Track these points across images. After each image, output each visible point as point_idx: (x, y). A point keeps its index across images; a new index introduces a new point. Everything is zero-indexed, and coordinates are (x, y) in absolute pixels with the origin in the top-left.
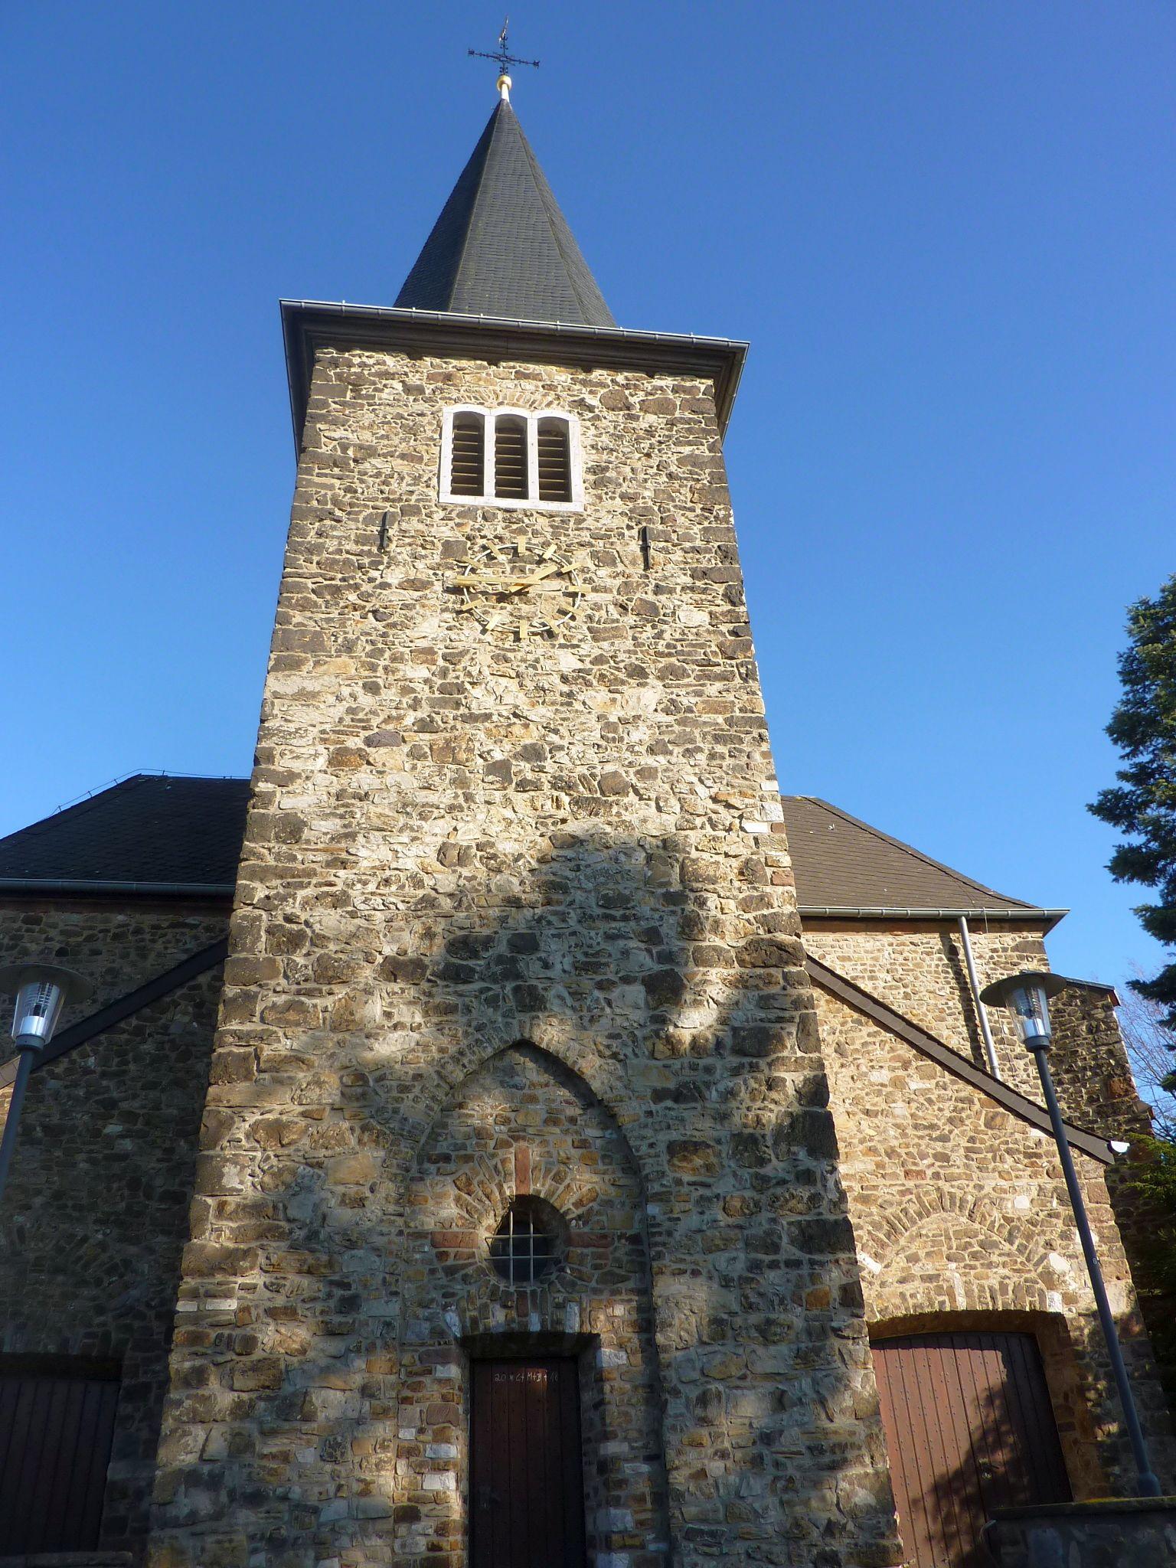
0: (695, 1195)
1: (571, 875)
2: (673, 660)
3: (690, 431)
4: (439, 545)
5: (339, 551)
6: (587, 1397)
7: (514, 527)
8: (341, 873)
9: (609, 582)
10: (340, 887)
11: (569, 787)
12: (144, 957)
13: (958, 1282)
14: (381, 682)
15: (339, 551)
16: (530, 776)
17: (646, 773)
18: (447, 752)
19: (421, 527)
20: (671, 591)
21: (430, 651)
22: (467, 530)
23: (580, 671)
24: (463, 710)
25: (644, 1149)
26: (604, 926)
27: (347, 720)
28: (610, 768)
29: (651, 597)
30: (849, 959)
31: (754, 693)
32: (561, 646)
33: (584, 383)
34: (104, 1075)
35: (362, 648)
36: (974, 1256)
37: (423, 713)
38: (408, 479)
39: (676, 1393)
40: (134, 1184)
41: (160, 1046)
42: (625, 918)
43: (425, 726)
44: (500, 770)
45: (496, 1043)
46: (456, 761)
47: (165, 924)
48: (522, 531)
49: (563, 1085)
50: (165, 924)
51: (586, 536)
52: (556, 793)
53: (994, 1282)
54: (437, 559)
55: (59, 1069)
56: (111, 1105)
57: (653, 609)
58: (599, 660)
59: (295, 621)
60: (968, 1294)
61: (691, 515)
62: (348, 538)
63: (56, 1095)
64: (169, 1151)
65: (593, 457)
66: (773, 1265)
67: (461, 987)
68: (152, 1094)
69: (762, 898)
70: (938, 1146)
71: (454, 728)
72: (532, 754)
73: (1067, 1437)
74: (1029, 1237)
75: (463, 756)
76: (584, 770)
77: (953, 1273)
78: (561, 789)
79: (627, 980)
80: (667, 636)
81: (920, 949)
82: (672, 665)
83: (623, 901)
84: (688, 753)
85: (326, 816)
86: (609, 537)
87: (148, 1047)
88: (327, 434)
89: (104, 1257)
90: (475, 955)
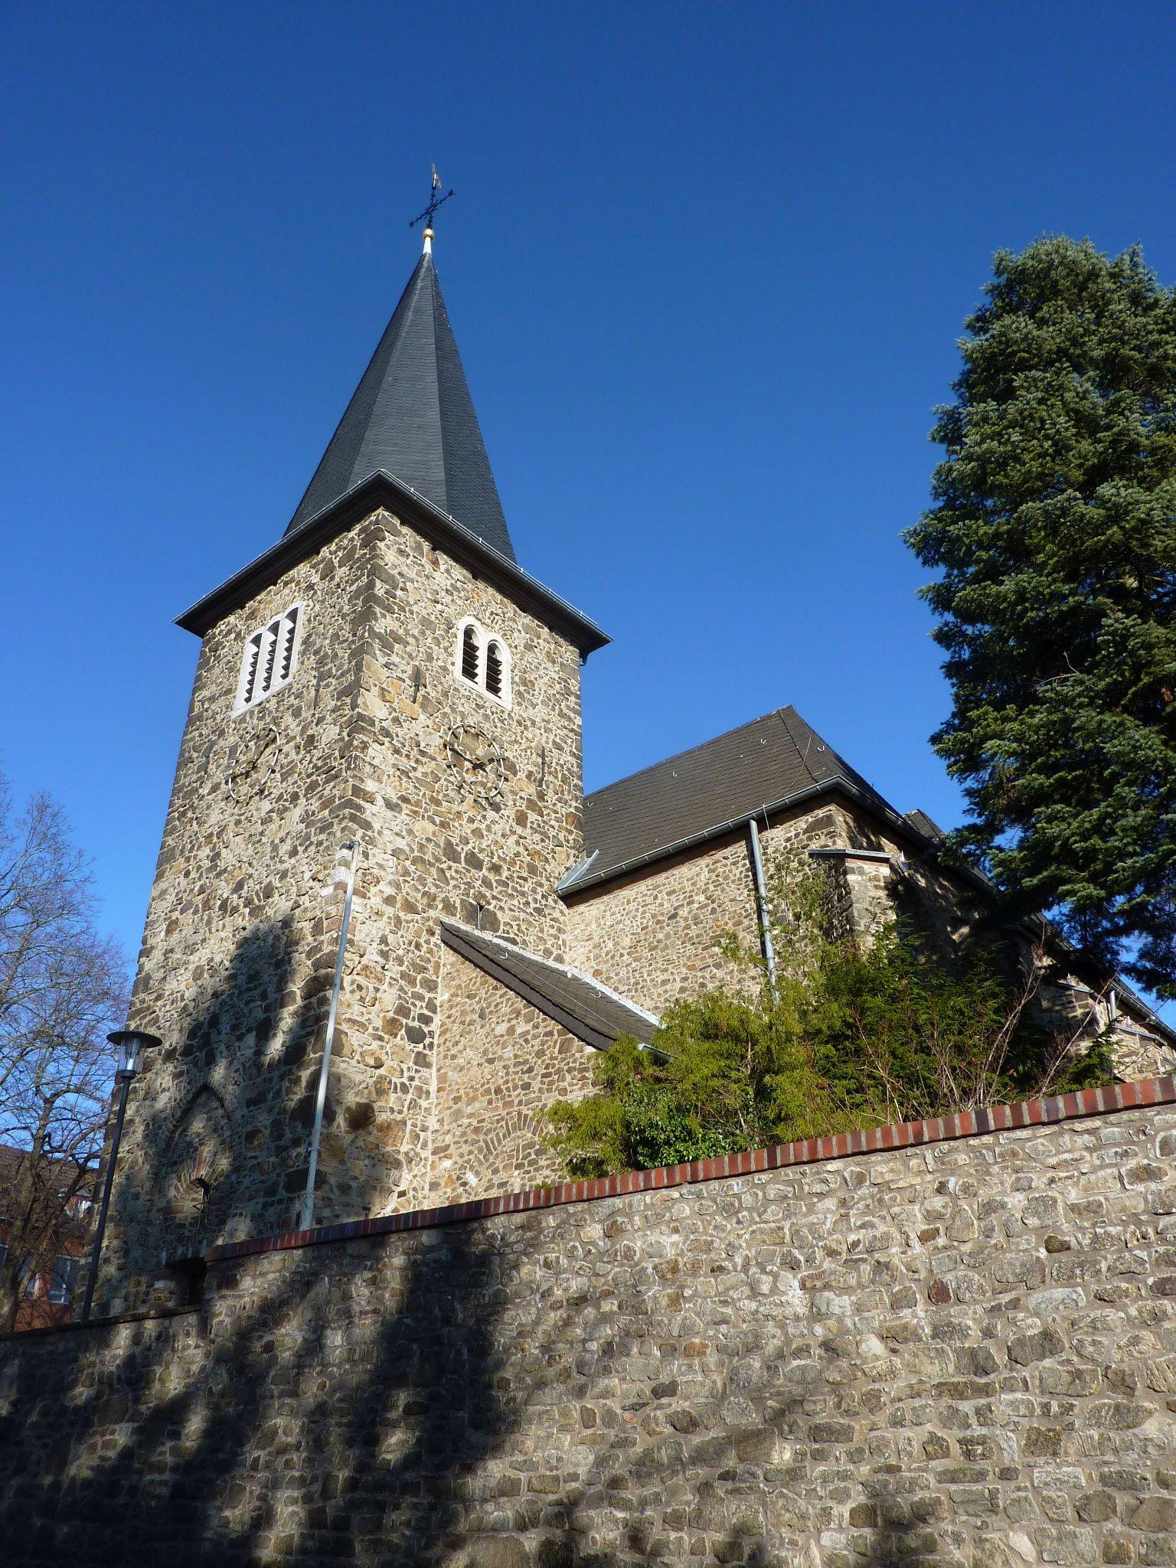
30: (674, 892)
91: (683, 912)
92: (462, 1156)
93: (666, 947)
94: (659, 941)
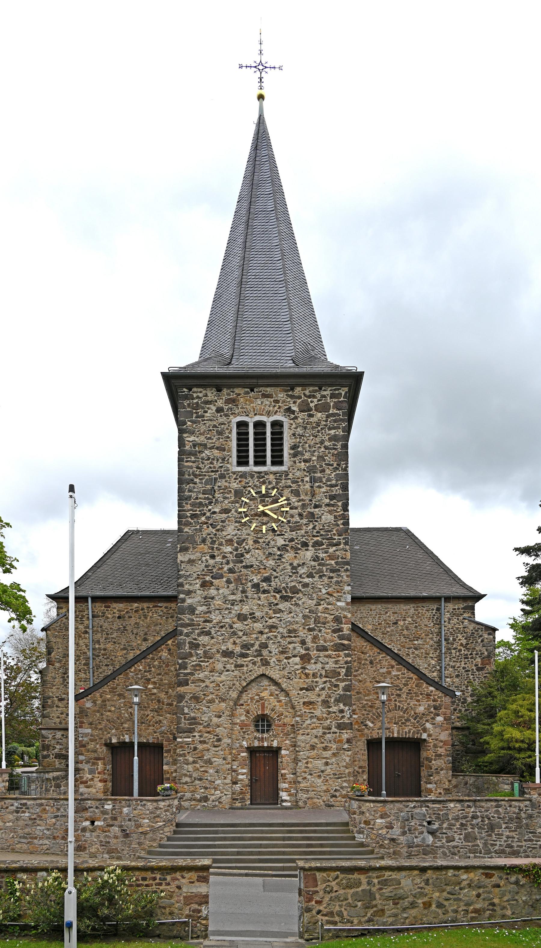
0: (309, 716)
1: (278, 622)
2: (318, 538)
3: (335, 421)
4: (233, 492)
5: (197, 498)
6: (279, 760)
7: (261, 480)
8: (208, 624)
9: (296, 504)
10: (208, 629)
11: (279, 592)
12: (146, 618)
13: (396, 730)
14: (215, 554)
15: (197, 498)
16: (266, 588)
17: (306, 585)
18: (238, 580)
19: (227, 484)
20: (321, 506)
21: (231, 540)
22: (243, 483)
23: (284, 545)
24: (244, 564)
25: (296, 704)
26: (288, 639)
27: (205, 569)
28: (293, 584)
29: (312, 510)
30: (396, 613)
31: (346, 551)
32: (278, 535)
33: (292, 397)
34: (145, 672)
35: (209, 540)
36: (402, 723)
37: (231, 565)
38: (220, 461)
39: (300, 761)
40: (159, 701)
41: (160, 663)
42: (295, 637)
43: (231, 571)
44: (256, 586)
45: (255, 675)
46: (242, 584)
47: (151, 606)
48: (264, 483)
49: (274, 685)
50: (151, 606)
51: (289, 482)
52: (275, 594)
53: (407, 730)
54: (233, 499)
55: (132, 670)
56: (148, 680)
57: (312, 515)
58: (292, 540)
59: (185, 531)
60: (398, 733)
61: (331, 467)
62: (199, 492)
63: (133, 677)
64: (167, 692)
65: (294, 440)
66: (329, 733)
67: (245, 659)
68: (160, 677)
69: (339, 629)
70: (398, 692)
71: (241, 571)
72: (267, 580)
73: (422, 768)
74: (421, 718)
75: (244, 582)
76: (284, 585)
77: (395, 728)
78: (277, 593)
79: (295, 656)
80: (317, 528)
81: (425, 609)
82: (318, 540)
83: (295, 631)
84: (320, 577)
85: (202, 606)
86: (298, 482)
87: (156, 663)
88: (187, 439)
89: (154, 720)
90: (249, 649)
91: (401, 623)
92: (363, 715)
93: (391, 635)
94: (388, 632)
